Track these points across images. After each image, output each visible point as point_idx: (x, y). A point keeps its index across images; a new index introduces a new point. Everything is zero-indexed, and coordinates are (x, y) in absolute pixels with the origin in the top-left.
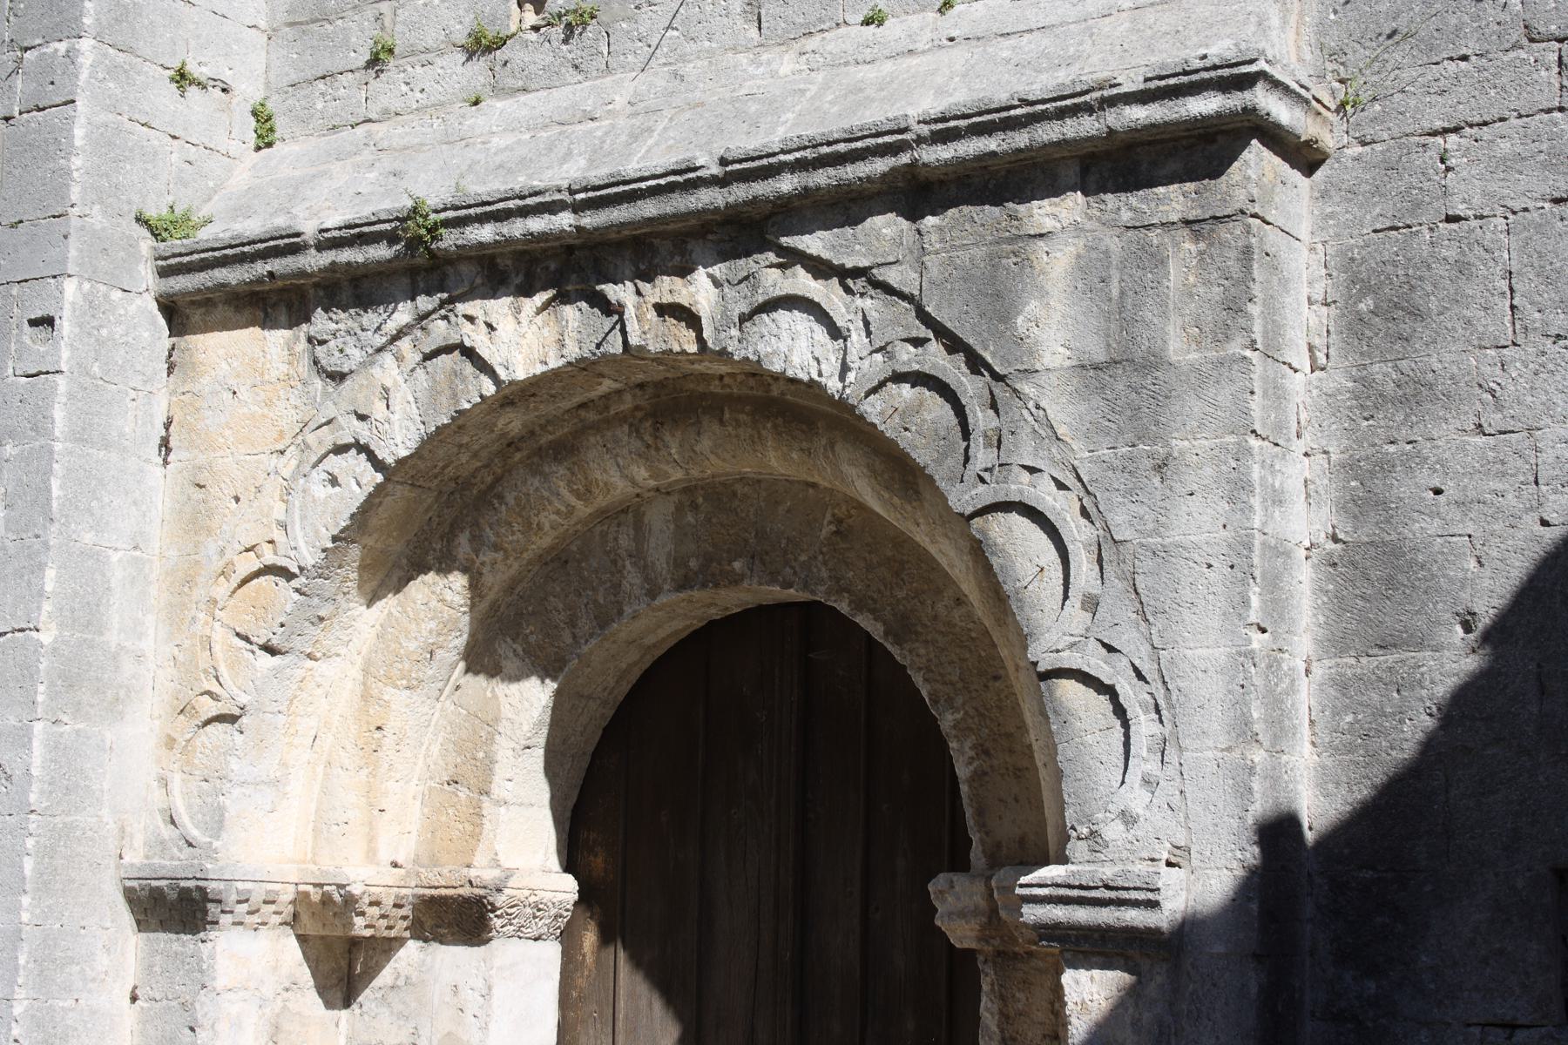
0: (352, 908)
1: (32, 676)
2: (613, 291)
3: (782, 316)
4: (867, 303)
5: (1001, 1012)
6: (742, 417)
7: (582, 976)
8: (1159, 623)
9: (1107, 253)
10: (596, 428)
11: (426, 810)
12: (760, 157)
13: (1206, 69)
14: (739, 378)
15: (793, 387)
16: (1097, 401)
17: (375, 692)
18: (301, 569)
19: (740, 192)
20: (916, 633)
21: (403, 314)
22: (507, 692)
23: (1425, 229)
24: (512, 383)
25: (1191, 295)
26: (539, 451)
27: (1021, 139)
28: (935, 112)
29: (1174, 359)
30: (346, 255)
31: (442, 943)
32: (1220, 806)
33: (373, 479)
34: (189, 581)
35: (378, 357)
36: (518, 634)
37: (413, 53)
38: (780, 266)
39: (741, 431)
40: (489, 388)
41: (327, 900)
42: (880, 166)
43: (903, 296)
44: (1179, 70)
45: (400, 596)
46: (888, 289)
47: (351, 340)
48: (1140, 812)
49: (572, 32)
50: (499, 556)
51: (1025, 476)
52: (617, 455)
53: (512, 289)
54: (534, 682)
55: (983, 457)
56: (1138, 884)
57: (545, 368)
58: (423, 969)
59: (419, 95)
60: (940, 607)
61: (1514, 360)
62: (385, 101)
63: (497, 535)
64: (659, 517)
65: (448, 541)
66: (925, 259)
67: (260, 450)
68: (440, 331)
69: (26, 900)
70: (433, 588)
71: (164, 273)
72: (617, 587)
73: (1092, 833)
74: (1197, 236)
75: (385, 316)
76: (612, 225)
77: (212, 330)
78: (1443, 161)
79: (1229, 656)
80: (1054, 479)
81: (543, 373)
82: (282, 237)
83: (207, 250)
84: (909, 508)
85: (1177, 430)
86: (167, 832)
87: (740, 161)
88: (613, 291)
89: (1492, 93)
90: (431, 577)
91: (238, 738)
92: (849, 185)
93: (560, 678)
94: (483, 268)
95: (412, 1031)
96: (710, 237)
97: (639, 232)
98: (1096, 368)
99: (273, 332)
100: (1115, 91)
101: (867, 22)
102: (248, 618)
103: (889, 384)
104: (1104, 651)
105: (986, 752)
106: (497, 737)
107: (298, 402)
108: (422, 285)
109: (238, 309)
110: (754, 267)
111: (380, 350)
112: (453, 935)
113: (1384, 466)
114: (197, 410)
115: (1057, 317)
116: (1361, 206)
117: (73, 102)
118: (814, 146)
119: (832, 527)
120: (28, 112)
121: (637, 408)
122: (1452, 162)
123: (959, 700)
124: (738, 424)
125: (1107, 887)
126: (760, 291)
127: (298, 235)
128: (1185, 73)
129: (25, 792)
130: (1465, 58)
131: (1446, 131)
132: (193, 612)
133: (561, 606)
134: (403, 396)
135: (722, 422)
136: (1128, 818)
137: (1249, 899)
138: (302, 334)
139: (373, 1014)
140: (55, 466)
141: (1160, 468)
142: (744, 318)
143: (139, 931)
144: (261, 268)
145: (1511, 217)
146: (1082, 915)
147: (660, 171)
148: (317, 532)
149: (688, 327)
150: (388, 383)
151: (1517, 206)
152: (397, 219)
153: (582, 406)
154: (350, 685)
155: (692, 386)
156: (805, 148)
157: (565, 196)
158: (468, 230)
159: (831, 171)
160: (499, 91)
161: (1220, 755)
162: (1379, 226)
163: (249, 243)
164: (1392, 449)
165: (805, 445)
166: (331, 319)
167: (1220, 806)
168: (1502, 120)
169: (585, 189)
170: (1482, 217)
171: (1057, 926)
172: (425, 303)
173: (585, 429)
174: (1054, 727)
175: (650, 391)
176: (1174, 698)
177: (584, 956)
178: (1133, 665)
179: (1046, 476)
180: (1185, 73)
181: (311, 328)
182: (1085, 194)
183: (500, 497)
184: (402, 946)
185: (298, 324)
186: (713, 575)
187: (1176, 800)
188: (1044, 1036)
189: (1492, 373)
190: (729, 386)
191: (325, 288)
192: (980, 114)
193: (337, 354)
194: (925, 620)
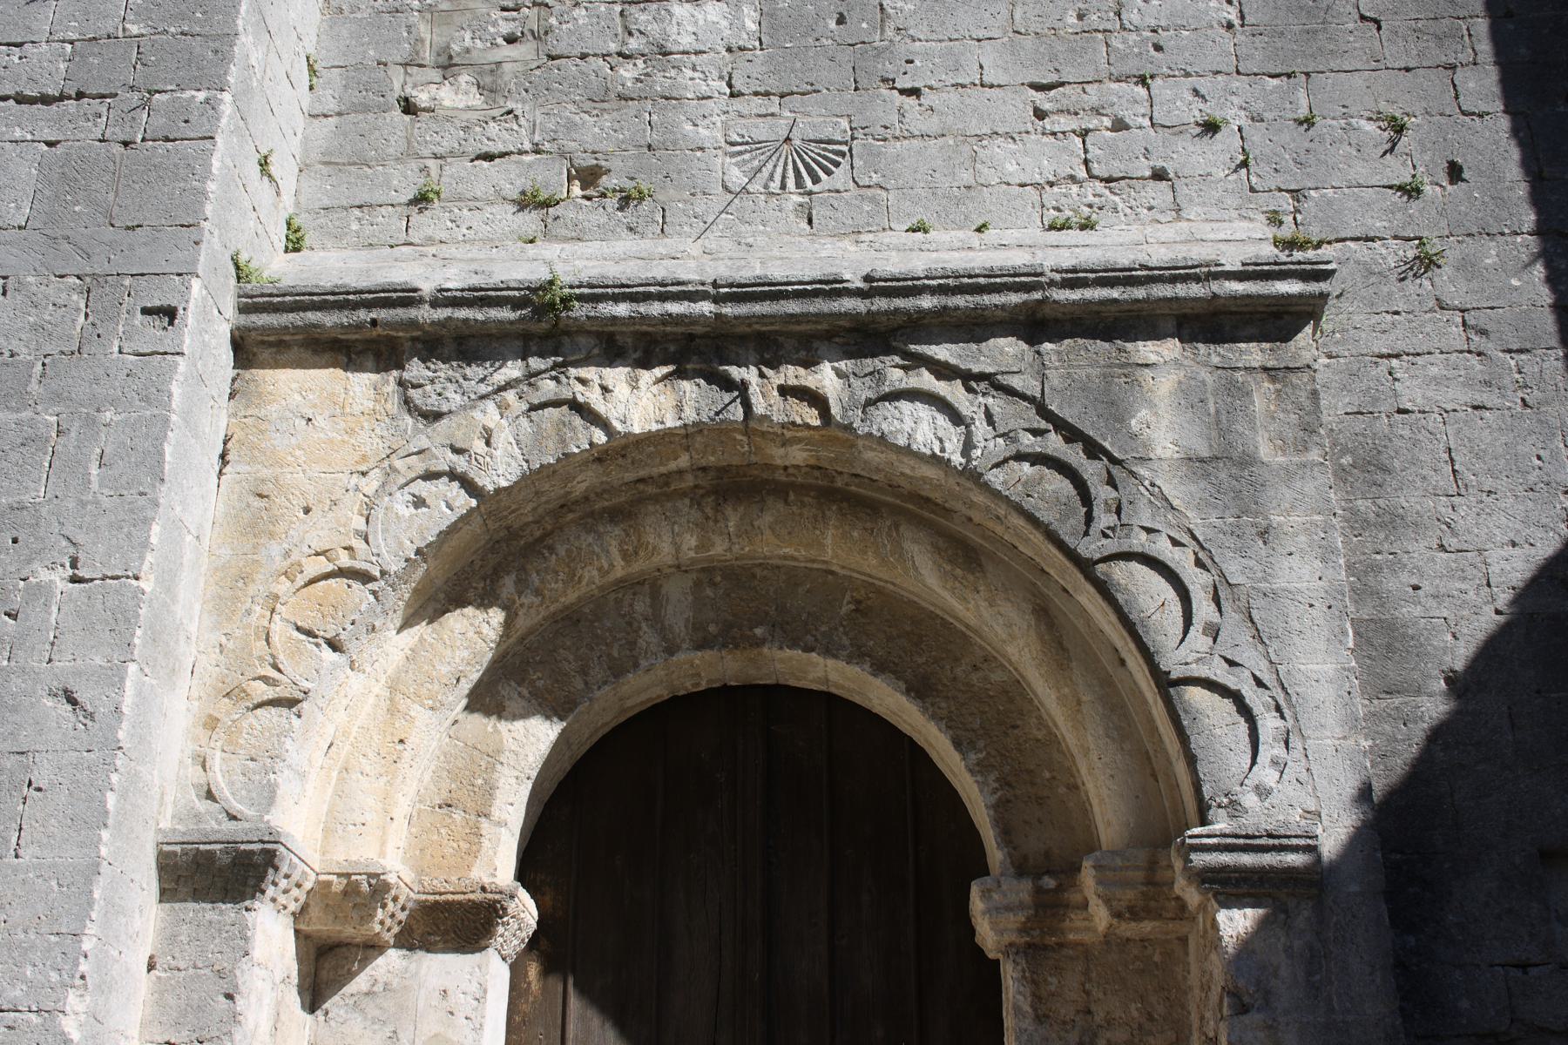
0: (379, 898)
1: (127, 620)
2: (736, 372)
3: (905, 405)
4: (990, 400)
5: (1034, 995)
6: (806, 499)
7: (527, 1002)
8: (1274, 646)
9: (1203, 382)
10: (655, 499)
11: (414, 830)
12: (905, 280)
13: (1292, 263)
14: (804, 470)
15: (857, 481)
16: (1203, 484)
17: (402, 707)
18: (383, 573)
19: (881, 304)
20: (937, 690)
21: (513, 370)
22: (512, 727)
23: (1383, 415)
24: (628, 435)
25: (1273, 418)
26: (592, 514)
27: (1139, 293)
28: (1066, 264)
29: (1265, 459)
30: (463, 313)
31: (428, 951)
32: (1342, 780)
33: (466, 504)
34: (245, 578)
35: (481, 404)
36: (523, 680)
37: (460, 200)
38: (903, 367)
39: (805, 512)
40: (600, 437)
41: (351, 890)
42: (1015, 298)
43: (1023, 397)
44: (1271, 260)
45: (435, 625)
46: (1010, 392)
47: (451, 387)
48: (1274, 785)
49: (627, 203)
50: (537, 601)
51: (1143, 536)
52: (675, 523)
53: (630, 361)
55: (1104, 519)
56: (1299, 833)
57: (660, 427)
58: (407, 975)
59: (465, 231)
60: (959, 671)
61: (1461, 505)
63: (542, 581)
64: (676, 591)
65: (492, 581)
66: (1047, 372)
67: (338, 469)
68: (548, 388)
69: (105, 835)
70: (471, 621)
71: (243, 310)
72: (632, 644)
73: (1231, 802)
74: (1273, 380)
75: (491, 370)
76: (754, 316)
77: (284, 367)
78: (1390, 374)
79: (1336, 670)
80: (1169, 537)
81: (658, 431)
82: (395, 291)
83: (304, 294)
84: (971, 578)
85: (1274, 508)
86: (203, 806)
87: (886, 280)
88: (736, 372)
89: (1421, 336)
90: (469, 610)
91: (296, 721)
92: (983, 310)
93: (570, 718)
94: (601, 343)
95: (389, 1034)
96: (837, 340)
97: (769, 328)
98: (1202, 461)
99: (356, 374)
100: (1220, 269)
102: (314, 614)
103: (1011, 462)
104: (1226, 666)
105: (1009, 784)
106: (499, 767)
107: (385, 433)
108: (534, 349)
109: (315, 352)
110: (880, 366)
111: (482, 397)
112: (446, 942)
113: (1376, 569)
114: (262, 432)
115: (1165, 422)
116: (1333, 397)
117: (212, 138)
118: (956, 277)
119: (852, 607)
120: (154, 140)
121: (696, 487)
122: (1398, 375)
123: (981, 744)
124: (803, 505)
125: (1270, 836)
126: (887, 383)
127: (415, 290)
128: (1276, 263)
129: (114, 729)
130: (1397, 313)
131: (1389, 356)
132: (248, 605)
133: (571, 657)
135: (786, 502)
136: (1262, 792)
137: (1375, 850)
138: (391, 379)
139: (341, 1020)
140: (169, 433)
141: (1264, 534)
142: (870, 403)
143: (160, 901)
144: (363, 315)
145: (1445, 415)
146: (1247, 859)
147: (807, 279)
148: (401, 544)
149: (810, 406)
150: (491, 425)
151: (1449, 408)
152: (528, 288)
153: (641, 480)
154: (371, 700)
155: (756, 472)
156: (948, 277)
157: (710, 289)
158: (601, 306)
159: (968, 298)
160: (547, 235)
161: (1337, 742)
162: (1349, 410)
163: (354, 293)
164: (1378, 557)
165: (869, 525)
166: (428, 368)
167: (1342, 780)
168: (1429, 353)
169: (731, 285)
170: (1424, 412)
171: (1225, 868)
172: (536, 363)
173: (641, 500)
174: (1185, 723)
175: (712, 474)
176: (1294, 699)
177: (529, 983)
178: (1254, 675)
179: (1164, 535)
180: (1276, 263)
181: (405, 374)
182: (1181, 341)
183: (551, 549)
184: (381, 954)
185: (387, 370)
186: (734, 638)
187: (1304, 776)
188: (1078, 1012)
189: (1446, 512)
190: (794, 475)
191: (425, 342)
192: (1106, 271)
193: (435, 397)
194: (945, 681)
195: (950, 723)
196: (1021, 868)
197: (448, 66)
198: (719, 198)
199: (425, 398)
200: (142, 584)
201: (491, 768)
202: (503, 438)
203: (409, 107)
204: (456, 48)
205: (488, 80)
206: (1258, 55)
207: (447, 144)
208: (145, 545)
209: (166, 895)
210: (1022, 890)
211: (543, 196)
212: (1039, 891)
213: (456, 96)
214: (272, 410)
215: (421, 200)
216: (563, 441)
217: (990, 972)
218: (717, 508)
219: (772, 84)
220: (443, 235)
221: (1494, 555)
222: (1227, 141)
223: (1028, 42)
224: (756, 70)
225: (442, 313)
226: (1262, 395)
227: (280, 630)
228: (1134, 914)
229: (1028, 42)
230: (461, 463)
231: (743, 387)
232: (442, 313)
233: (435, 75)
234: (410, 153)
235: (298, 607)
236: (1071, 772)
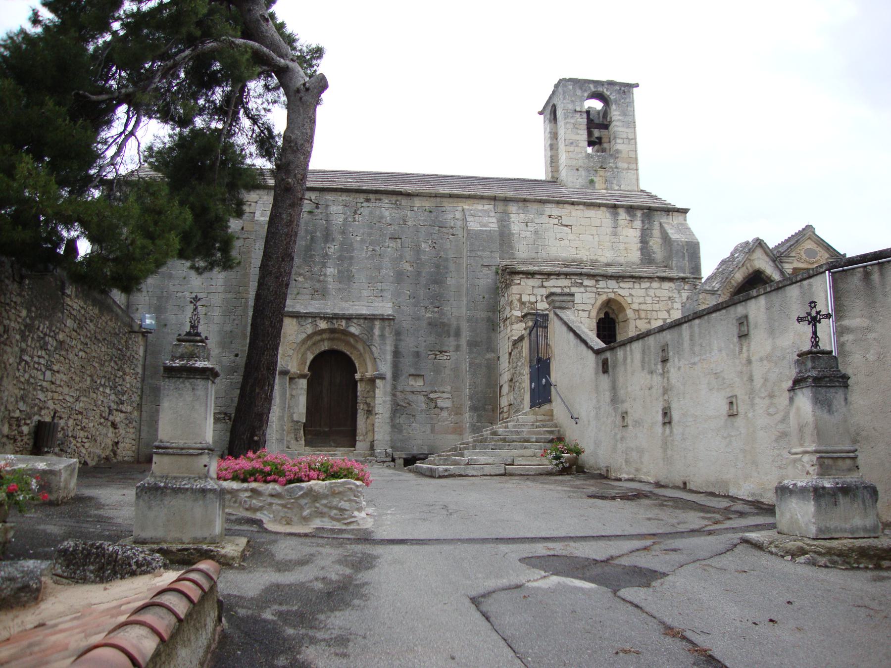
215: (298, 294)
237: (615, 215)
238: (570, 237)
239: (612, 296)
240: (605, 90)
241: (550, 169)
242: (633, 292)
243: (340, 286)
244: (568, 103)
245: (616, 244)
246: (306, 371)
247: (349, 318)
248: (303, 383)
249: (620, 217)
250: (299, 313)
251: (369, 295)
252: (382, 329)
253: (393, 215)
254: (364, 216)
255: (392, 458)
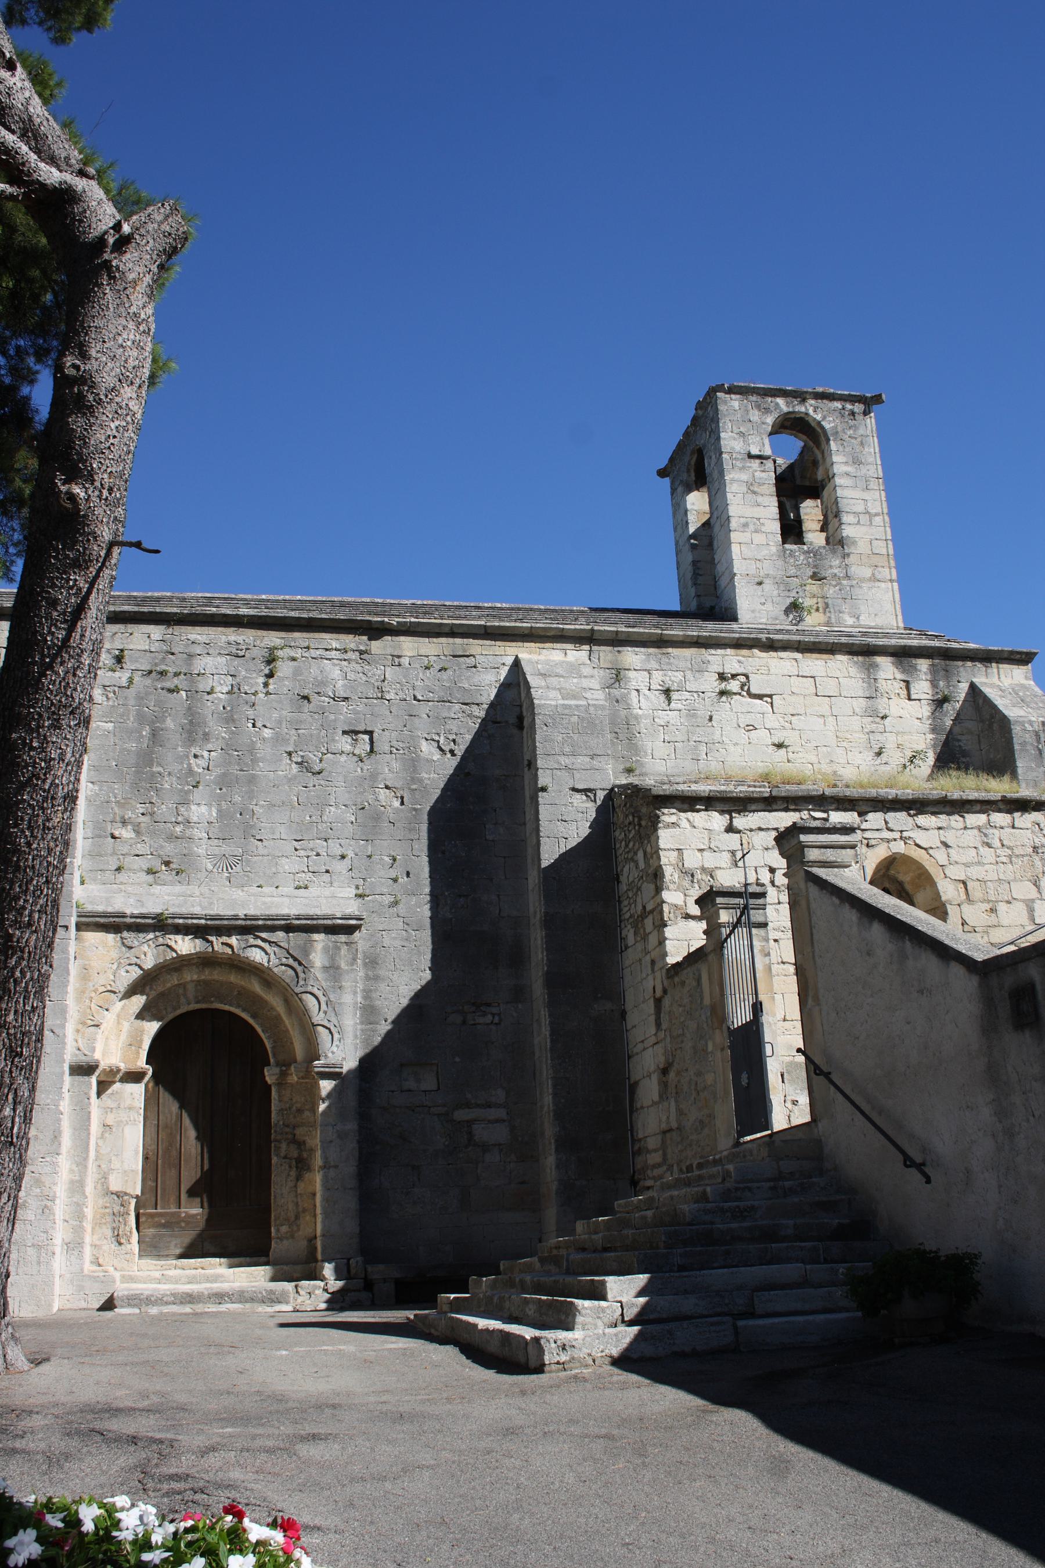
2: (210, 938)
3: (253, 948)
8: (339, 1017)
10: (186, 965)
19: (249, 922)
21: (151, 935)
28: (297, 913)
30: (138, 920)
34: (83, 992)
40: (175, 955)
42: (283, 922)
54: (155, 1022)
55: (301, 982)
62: (121, 880)
64: (191, 988)
71: (78, 916)
86: (77, 1052)
88: (210, 938)
101: (258, 887)
113: (371, 991)
134: (149, 955)
136: (333, 1053)
141: (340, 988)
144: (112, 920)
146: (327, 1070)
160: (156, 883)
171: (322, 1072)
172: (157, 934)
195: (261, 1025)
196: (277, 1064)
197: (124, 822)
198: (204, 874)
199: (128, 942)
200: (67, 1002)
201: (142, 1035)
202: (149, 955)
203: (113, 837)
204: (126, 817)
205: (136, 828)
206: (359, 833)
207: (125, 850)
208: (67, 992)
209: (71, 1074)
210: (277, 1070)
211: (154, 870)
212: (281, 1071)
213: (127, 833)
214: (87, 944)
215: (119, 869)
216: (165, 956)
217: (268, 1088)
218: (203, 969)
219: (220, 836)
220: (125, 881)
221: (401, 988)
222: (347, 861)
223: (294, 825)
224: (216, 830)
225: (133, 920)
226: (344, 950)
227: (93, 1005)
228: (303, 1078)
229: (294, 825)
230: (138, 962)
231: (212, 942)
232: (133, 920)
233: (120, 825)
234: (114, 853)
235: (97, 999)
236: (291, 1039)
237: (870, 669)
238: (772, 721)
239: (899, 847)
240: (811, 411)
241: (692, 591)
242: (950, 837)
243: (226, 849)
244: (735, 439)
245: (878, 736)
246: (141, 1062)
247: (248, 928)
248: (136, 1093)
249: (881, 675)
250: (123, 916)
251: (296, 868)
252: (332, 954)
253: (351, 676)
254: (282, 679)
255: (366, 1279)
